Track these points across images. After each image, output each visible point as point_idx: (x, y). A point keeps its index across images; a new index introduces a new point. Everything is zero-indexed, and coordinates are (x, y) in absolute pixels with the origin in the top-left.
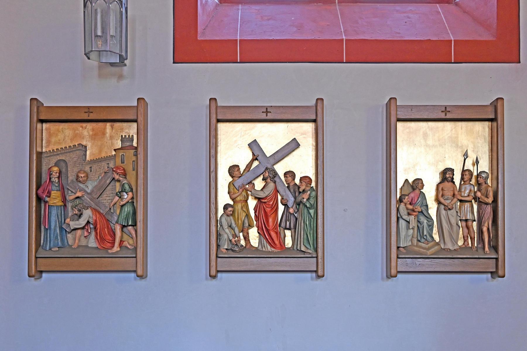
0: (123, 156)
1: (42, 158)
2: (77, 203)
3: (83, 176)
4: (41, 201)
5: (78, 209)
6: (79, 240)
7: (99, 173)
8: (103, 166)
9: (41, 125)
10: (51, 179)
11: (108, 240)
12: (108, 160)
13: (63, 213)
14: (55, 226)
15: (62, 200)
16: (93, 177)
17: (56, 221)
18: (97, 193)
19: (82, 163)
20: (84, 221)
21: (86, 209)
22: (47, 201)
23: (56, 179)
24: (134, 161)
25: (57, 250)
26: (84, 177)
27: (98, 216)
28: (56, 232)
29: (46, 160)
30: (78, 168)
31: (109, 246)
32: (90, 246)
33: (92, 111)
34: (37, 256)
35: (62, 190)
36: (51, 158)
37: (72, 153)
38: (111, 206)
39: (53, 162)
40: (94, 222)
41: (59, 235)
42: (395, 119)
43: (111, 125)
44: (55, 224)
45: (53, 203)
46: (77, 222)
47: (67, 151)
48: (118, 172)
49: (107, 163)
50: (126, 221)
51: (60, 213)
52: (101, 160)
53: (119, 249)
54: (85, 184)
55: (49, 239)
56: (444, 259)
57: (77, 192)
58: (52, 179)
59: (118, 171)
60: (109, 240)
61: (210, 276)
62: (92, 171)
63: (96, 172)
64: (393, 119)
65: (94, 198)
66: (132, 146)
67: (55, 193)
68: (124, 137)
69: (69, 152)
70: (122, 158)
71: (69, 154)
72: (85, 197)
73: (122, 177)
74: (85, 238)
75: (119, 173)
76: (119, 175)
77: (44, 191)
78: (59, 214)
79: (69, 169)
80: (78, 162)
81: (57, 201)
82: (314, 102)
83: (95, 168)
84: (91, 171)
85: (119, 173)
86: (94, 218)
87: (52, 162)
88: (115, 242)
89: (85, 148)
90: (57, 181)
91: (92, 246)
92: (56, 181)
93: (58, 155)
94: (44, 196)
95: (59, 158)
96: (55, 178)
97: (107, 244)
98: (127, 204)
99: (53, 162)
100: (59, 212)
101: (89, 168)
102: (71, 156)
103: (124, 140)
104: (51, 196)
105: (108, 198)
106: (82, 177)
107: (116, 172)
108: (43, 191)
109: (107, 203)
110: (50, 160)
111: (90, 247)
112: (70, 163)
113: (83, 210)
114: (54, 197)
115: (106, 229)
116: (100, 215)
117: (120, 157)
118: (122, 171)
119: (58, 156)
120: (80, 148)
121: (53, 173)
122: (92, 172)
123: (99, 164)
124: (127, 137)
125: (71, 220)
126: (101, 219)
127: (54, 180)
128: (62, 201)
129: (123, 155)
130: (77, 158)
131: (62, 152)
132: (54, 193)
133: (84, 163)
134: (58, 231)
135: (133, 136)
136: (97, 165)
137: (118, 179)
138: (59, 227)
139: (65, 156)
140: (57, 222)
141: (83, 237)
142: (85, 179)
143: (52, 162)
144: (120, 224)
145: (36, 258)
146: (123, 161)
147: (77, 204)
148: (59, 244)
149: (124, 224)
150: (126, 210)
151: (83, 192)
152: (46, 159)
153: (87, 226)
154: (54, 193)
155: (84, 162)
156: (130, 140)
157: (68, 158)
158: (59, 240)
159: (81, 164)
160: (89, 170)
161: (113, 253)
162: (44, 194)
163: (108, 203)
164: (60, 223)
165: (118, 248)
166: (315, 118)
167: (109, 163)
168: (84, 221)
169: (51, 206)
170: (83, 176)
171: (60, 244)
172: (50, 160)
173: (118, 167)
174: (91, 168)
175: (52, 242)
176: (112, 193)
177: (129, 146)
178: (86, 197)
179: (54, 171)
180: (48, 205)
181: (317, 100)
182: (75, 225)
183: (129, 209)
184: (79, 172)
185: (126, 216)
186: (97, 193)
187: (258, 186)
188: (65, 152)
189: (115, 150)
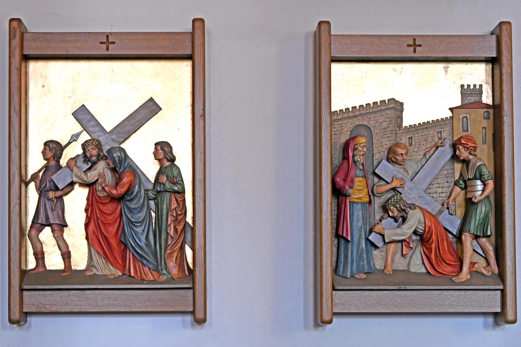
0: (465, 119)
7: (425, 148)
8: (430, 135)
10: (354, 157)
12: (439, 127)
14: (360, 237)
16: (414, 154)
22: (350, 194)
24: (485, 128)
25: (365, 278)
28: (361, 247)
29: (336, 126)
30: (389, 139)
31: (450, 270)
32: (412, 270)
33: (420, 44)
34: (25, 287)
36: (345, 123)
37: (378, 114)
39: (347, 128)
42: (328, 59)
43: (443, 67)
45: (357, 198)
46: (398, 231)
47: (371, 110)
49: (438, 130)
52: (428, 126)
55: (350, 259)
56: (454, 291)
61: (11, 321)
63: (419, 146)
64: (325, 57)
66: (480, 102)
67: (361, 181)
68: (466, 87)
69: (375, 113)
71: (374, 115)
75: (471, 148)
79: (375, 142)
80: (390, 129)
81: (363, 194)
82: (189, 28)
83: (418, 140)
85: (471, 148)
86: (427, 223)
87: (345, 130)
89: (400, 105)
91: (417, 271)
93: (356, 117)
95: (357, 122)
97: (446, 267)
99: (347, 128)
101: (407, 139)
103: (467, 92)
104: (355, 186)
105: (440, 190)
108: (344, 178)
109: (438, 198)
110: (342, 125)
111: (413, 273)
112: (376, 131)
113: (409, 209)
114: (359, 188)
117: (461, 120)
119: (355, 119)
121: (360, 148)
123: (424, 134)
124: (472, 87)
127: (359, 160)
130: (388, 123)
131: (362, 112)
132: (359, 182)
133: (400, 132)
135: (481, 86)
136: (421, 134)
137: (466, 157)
139: (367, 119)
143: (345, 130)
144: (473, 234)
145: (22, 290)
147: (398, 200)
152: (336, 123)
154: (359, 182)
155: (400, 130)
156: (476, 92)
157: (372, 122)
161: (463, 282)
162: (346, 184)
163: (441, 199)
166: (191, 53)
167: (441, 132)
169: (353, 202)
172: (342, 125)
176: (447, 182)
177: (475, 102)
179: (361, 143)
180: (350, 202)
181: (320, 23)
188: (367, 113)
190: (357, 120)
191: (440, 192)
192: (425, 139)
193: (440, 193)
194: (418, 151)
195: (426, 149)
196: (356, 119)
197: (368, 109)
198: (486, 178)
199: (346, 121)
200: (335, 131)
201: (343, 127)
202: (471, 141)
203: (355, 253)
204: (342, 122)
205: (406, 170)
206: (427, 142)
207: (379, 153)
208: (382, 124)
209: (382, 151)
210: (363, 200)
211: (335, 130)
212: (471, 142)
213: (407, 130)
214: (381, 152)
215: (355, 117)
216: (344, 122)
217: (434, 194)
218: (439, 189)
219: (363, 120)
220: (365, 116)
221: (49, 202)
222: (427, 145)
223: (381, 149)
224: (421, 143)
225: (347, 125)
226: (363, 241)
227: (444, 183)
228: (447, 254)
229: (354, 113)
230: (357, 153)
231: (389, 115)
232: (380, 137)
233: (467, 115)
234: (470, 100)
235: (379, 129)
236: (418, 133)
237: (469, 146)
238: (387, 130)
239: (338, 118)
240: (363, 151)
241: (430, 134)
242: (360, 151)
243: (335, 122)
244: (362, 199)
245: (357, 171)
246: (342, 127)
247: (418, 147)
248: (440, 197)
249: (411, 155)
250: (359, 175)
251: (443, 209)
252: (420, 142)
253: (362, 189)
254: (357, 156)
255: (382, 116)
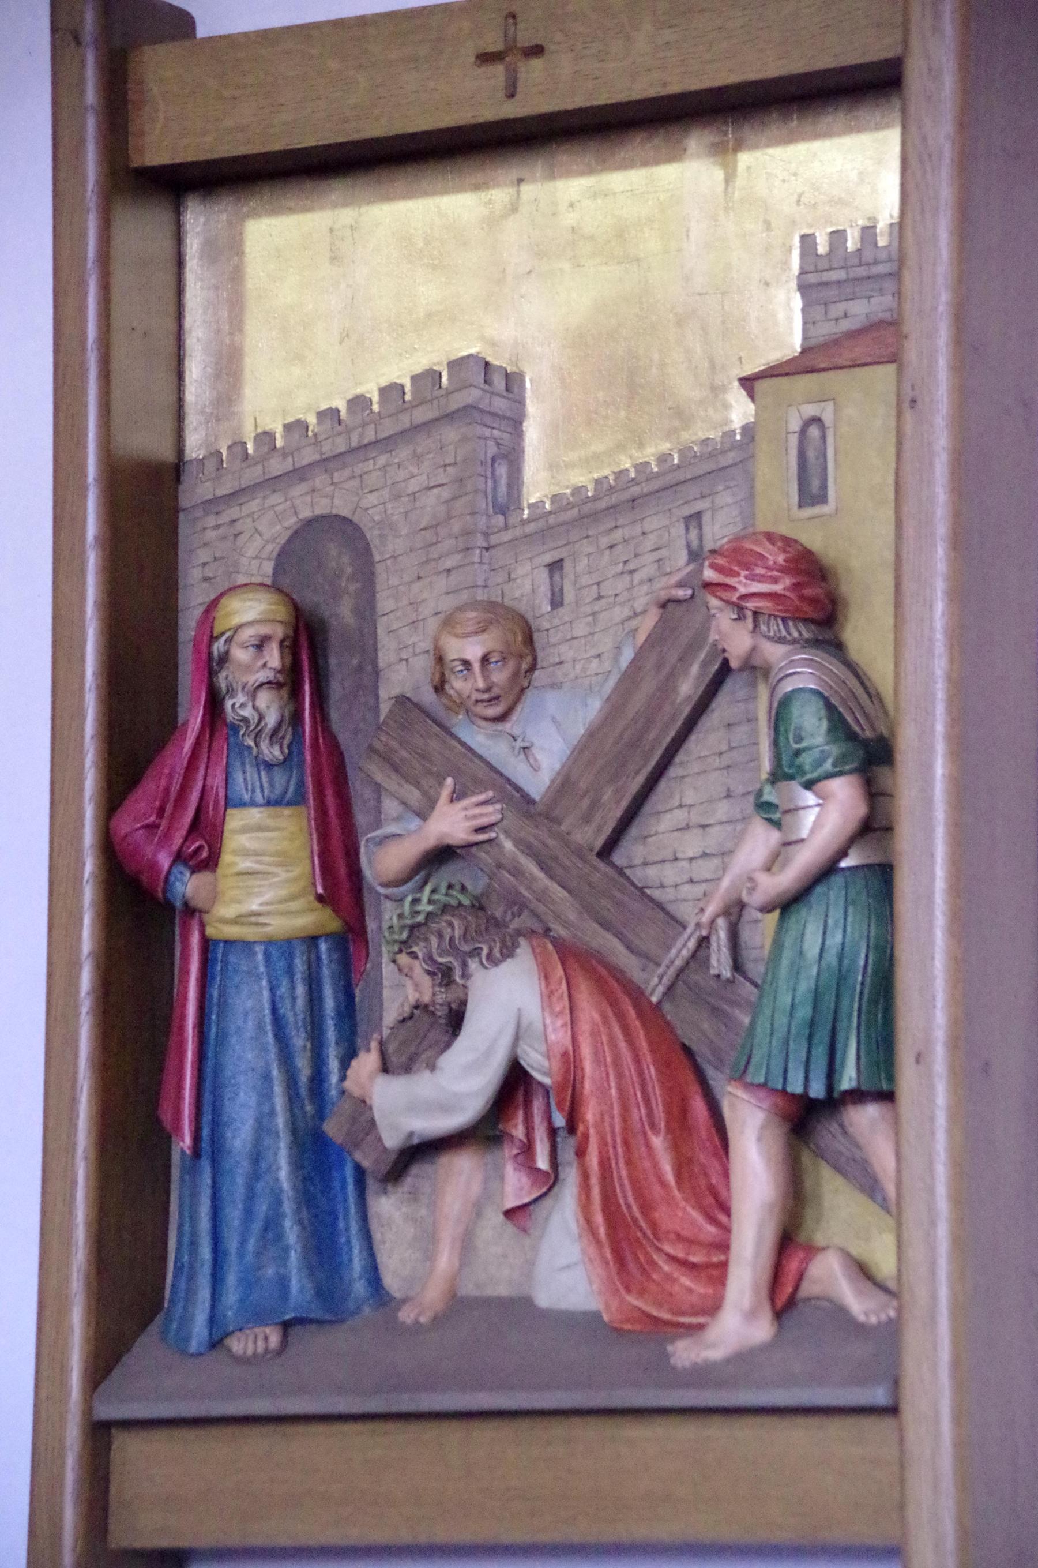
1: (182, 516)
2: (425, 907)
3: (473, 651)
4: (456, 852)
5: (430, 958)
6: (466, 1245)
7: (627, 612)
9: (168, 230)
10: (536, 669)
11: (680, 1238)
12: (693, 490)
13: (329, 1004)
14: (263, 1128)
15: (314, 885)
16: (571, 654)
17: (267, 1077)
18: (595, 805)
19: (486, 535)
20: (471, 1068)
21: (489, 956)
23: (264, 698)
26: (485, 660)
27: (589, 1011)
32: (543, 1300)
35: (329, 793)
37: (403, 453)
38: (713, 922)
39: (258, 542)
40: (556, 1065)
41: (298, 1211)
44: (260, 1104)
48: (744, 597)
49: (687, 511)
50: (820, 1053)
51: (301, 1002)
53: (763, 1330)
54: (507, 726)
57: (431, 803)
58: (228, 704)
59: (744, 586)
60: (690, 1242)
62: (569, 596)
65: (579, 852)
68: (822, 249)
70: (811, 454)
71: (382, 460)
72: (500, 846)
73: (781, 640)
74: (510, 1229)
75: (751, 605)
76: (756, 624)
77: (161, 812)
78: (296, 1010)
80: (456, 527)
81: (268, 896)
84: (557, 602)
85: (751, 605)
86: (552, 1037)
87: (251, 552)
88: (724, 1265)
90: (271, 720)
92: (261, 718)
93: (302, 479)
94: (164, 860)
96: (253, 694)
98: (819, 889)
99: (258, 542)
100: (294, 999)
101: (543, 575)
102: (402, 474)
104: (226, 857)
106: (466, 663)
107: (726, 595)
109: (687, 888)
115: (658, 1142)
116: (613, 1003)
117: (794, 440)
118: (775, 581)
119: (298, 490)
120: (469, 400)
122: (561, 611)
123: (618, 535)
125: (394, 1060)
126: (612, 1039)
127: (247, 712)
128: (320, 898)
129: (817, 420)
130: (445, 493)
133: (506, 536)
134: (284, 1173)
136: (604, 541)
138: (294, 1131)
140: (278, 1089)
141: (494, 1218)
142: (500, 676)
143: (251, 552)
144: (763, 1086)
146: (815, 484)
147: (420, 918)
148: (294, 1285)
149: (796, 1087)
150: (812, 946)
151: (486, 803)
153: (520, 1114)
154: (245, 830)
155: (506, 527)
157: (372, 499)
158: (294, 1256)
159: (481, 542)
160: (544, 589)
164: (304, 1091)
165: (751, 1315)
167: (699, 515)
168: (471, 1068)
170: (473, 651)
171: (302, 1291)
172: (239, 526)
173: (748, 545)
174: (557, 577)
175: (231, 1279)
178: (508, 845)
179: (241, 626)
180: (206, 944)
182: (413, 1108)
183: (835, 939)
184: (448, 622)
185: (815, 1008)
186: (595, 805)
187: (400, 970)
189: (748, 383)
190: (307, 493)
191: (691, 854)
192: (625, 562)
193: (691, 859)
194: (592, 634)
195: (629, 618)
196: (303, 488)
197: (354, 429)
198: (807, 767)
199: (257, 501)
200: (204, 564)
201: (242, 539)
202: (747, 567)
203: (630, 1194)
204: (238, 508)
205: (519, 744)
206: (636, 582)
207: (404, 662)
208: (418, 504)
209: (418, 651)
210: (268, 929)
211: (205, 560)
212: (744, 573)
213: (541, 524)
214: (415, 655)
215: (299, 474)
216: (246, 510)
217: (667, 865)
218: (688, 836)
219: (332, 488)
220: (344, 466)
221: (295, 888)
222: (634, 599)
223: (414, 639)
224: (607, 589)
225: (260, 528)
226: (279, 1148)
227: (710, 801)
228: (677, 1205)
229: (290, 459)
230: (230, 677)
231: (451, 447)
232: (406, 578)
233: (823, 410)
234: (846, 316)
235: (404, 532)
236: (590, 533)
237: (737, 595)
238: (442, 532)
239: (219, 493)
240: (265, 665)
241: (651, 536)
242: (248, 668)
243: (207, 513)
244: (262, 920)
245: (238, 777)
246: (236, 536)
247: (594, 614)
248: (691, 881)
249: (557, 660)
250: (246, 797)
251: (679, 951)
252: (598, 583)
253: (257, 867)
254: (232, 697)
255: (418, 458)
